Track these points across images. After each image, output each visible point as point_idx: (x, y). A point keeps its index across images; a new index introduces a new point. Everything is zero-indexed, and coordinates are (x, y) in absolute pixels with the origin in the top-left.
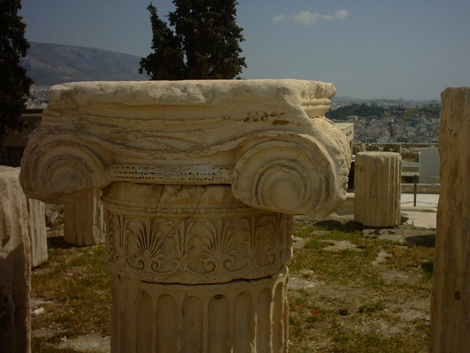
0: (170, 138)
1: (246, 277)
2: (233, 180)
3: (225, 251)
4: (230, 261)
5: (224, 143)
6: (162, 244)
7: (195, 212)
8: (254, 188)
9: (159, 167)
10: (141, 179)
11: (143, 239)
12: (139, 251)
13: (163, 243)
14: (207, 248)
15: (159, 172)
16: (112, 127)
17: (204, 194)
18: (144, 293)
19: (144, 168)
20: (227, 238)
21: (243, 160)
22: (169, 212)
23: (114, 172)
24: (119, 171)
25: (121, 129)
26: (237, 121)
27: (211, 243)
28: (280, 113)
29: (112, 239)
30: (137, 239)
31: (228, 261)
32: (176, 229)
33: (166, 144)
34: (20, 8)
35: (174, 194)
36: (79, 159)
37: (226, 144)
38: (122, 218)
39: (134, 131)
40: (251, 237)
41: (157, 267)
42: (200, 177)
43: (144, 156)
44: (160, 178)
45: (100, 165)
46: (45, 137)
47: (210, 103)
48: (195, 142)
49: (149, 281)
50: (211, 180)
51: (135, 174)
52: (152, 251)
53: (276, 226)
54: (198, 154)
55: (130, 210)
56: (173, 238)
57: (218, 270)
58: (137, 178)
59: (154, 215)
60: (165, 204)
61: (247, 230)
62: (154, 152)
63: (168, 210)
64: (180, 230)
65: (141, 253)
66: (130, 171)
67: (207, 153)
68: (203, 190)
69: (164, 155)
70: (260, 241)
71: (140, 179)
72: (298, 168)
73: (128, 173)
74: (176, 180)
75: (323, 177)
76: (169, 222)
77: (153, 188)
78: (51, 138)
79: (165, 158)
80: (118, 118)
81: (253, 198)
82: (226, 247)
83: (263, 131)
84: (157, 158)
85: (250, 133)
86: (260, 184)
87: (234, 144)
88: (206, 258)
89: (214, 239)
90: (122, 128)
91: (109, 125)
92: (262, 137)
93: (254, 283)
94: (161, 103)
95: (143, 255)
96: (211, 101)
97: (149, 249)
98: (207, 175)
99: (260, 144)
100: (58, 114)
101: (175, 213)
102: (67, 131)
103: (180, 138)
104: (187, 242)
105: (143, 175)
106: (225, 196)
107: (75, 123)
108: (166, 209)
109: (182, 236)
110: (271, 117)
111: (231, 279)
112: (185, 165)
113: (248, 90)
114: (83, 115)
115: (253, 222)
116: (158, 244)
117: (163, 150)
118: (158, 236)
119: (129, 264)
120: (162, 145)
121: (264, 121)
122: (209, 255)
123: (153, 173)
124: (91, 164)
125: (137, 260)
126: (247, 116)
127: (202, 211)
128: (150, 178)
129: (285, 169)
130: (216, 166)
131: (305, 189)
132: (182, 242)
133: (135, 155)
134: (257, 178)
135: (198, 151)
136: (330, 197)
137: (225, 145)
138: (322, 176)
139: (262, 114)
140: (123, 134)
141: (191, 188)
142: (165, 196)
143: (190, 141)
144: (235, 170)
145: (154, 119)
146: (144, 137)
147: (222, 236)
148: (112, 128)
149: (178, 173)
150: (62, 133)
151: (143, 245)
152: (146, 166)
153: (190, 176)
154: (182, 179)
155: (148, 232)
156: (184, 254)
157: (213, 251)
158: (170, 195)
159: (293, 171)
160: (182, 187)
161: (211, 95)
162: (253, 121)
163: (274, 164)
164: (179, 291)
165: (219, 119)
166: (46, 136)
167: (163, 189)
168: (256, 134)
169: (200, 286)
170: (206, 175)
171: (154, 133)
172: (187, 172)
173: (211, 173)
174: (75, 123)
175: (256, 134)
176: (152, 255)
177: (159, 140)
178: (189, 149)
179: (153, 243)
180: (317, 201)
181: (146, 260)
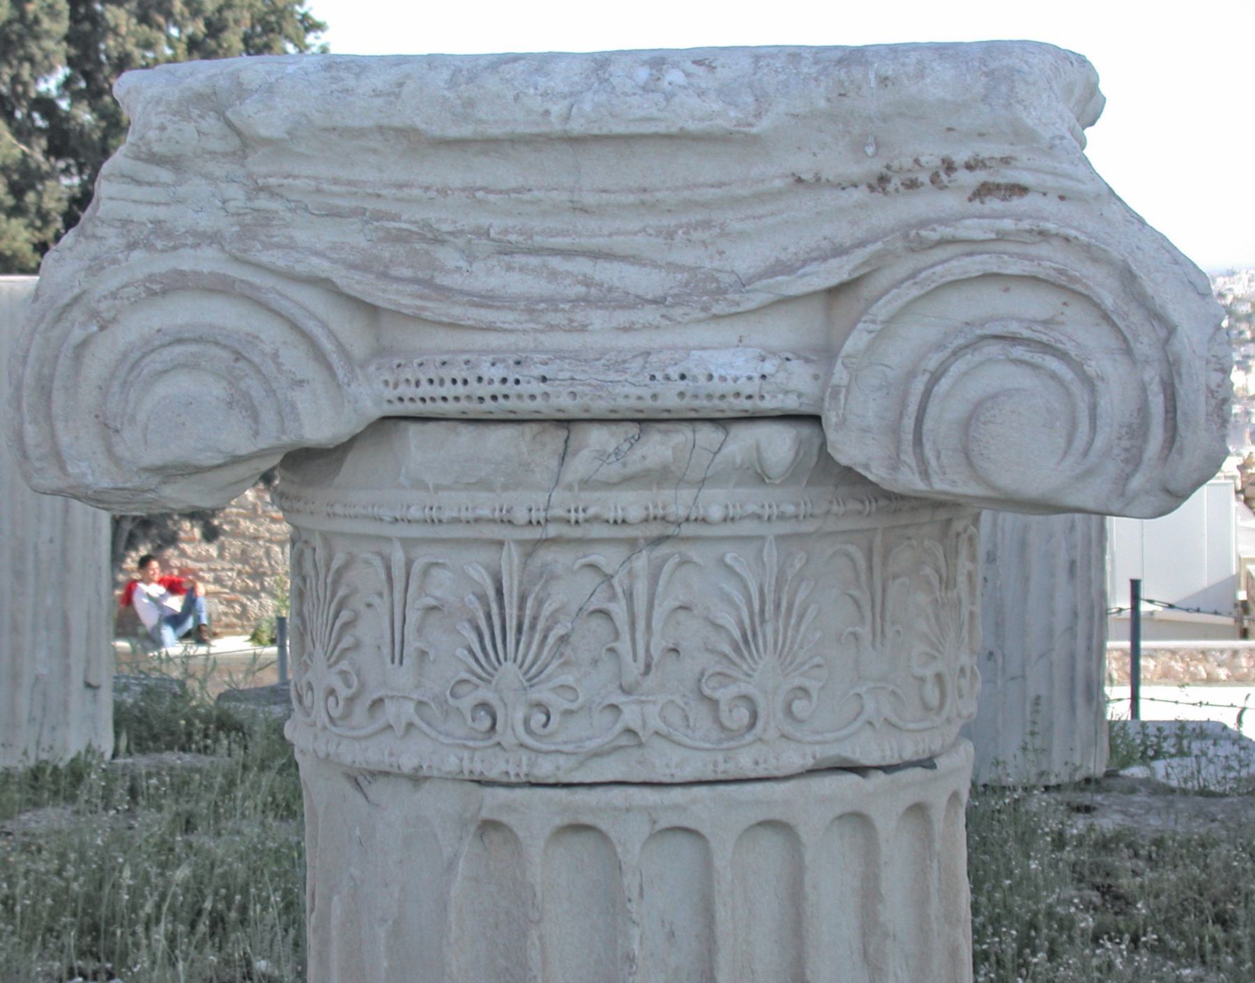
3: (789, 659)
6: (563, 639)
8: (909, 423)
9: (565, 358)
10: (501, 400)
15: (567, 375)
16: (377, 220)
19: (511, 362)
21: (872, 327)
23: (386, 383)
24: (409, 377)
25: (414, 228)
26: (843, 189)
27: (744, 636)
30: (467, 625)
33: (580, 277)
35: (616, 454)
36: (852, 560)
37: (808, 269)
39: (462, 232)
41: (545, 725)
43: (504, 323)
44: (573, 394)
46: (115, 261)
47: (750, 125)
48: (690, 268)
49: (513, 779)
52: (526, 665)
54: (705, 309)
55: (440, 521)
58: (481, 399)
59: (536, 533)
62: (543, 305)
65: (484, 675)
66: (455, 373)
69: (579, 316)
71: (493, 403)
73: (448, 383)
74: (632, 402)
75: (1152, 379)
77: (534, 437)
78: (143, 264)
79: (583, 328)
81: (903, 457)
83: (942, 221)
84: (552, 328)
85: (893, 231)
90: (416, 222)
91: (364, 214)
93: (879, 778)
95: (490, 682)
96: (751, 119)
97: (515, 661)
98: (743, 380)
100: (166, 175)
101: (615, 522)
103: (634, 257)
104: (657, 625)
105: (509, 388)
107: (232, 206)
108: (584, 510)
110: (967, 172)
113: (886, 78)
114: (265, 177)
116: (551, 640)
117: (573, 297)
118: (547, 609)
120: (568, 282)
121: (943, 188)
123: (544, 379)
125: (466, 703)
128: (533, 397)
133: (469, 319)
134: (919, 386)
135: (705, 298)
136: (1177, 444)
137: (804, 275)
143: (673, 267)
144: (839, 362)
145: (539, 189)
146: (500, 253)
148: (376, 224)
149: (641, 378)
150: (185, 245)
152: (515, 357)
153: (682, 385)
156: (648, 667)
157: (749, 660)
161: (750, 99)
162: (901, 189)
164: (628, 810)
166: (120, 256)
168: (917, 234)
169: (703, 791)
170: (739, 382)
172: (674, 372)
173: (756, 375)
174: (232, 206)
175: (917, 234)
176: (529, 680)
177: (555, 262)
178: (671, 292)
179: (531, 638)
180: (1134, 461)
181: (502, 699)
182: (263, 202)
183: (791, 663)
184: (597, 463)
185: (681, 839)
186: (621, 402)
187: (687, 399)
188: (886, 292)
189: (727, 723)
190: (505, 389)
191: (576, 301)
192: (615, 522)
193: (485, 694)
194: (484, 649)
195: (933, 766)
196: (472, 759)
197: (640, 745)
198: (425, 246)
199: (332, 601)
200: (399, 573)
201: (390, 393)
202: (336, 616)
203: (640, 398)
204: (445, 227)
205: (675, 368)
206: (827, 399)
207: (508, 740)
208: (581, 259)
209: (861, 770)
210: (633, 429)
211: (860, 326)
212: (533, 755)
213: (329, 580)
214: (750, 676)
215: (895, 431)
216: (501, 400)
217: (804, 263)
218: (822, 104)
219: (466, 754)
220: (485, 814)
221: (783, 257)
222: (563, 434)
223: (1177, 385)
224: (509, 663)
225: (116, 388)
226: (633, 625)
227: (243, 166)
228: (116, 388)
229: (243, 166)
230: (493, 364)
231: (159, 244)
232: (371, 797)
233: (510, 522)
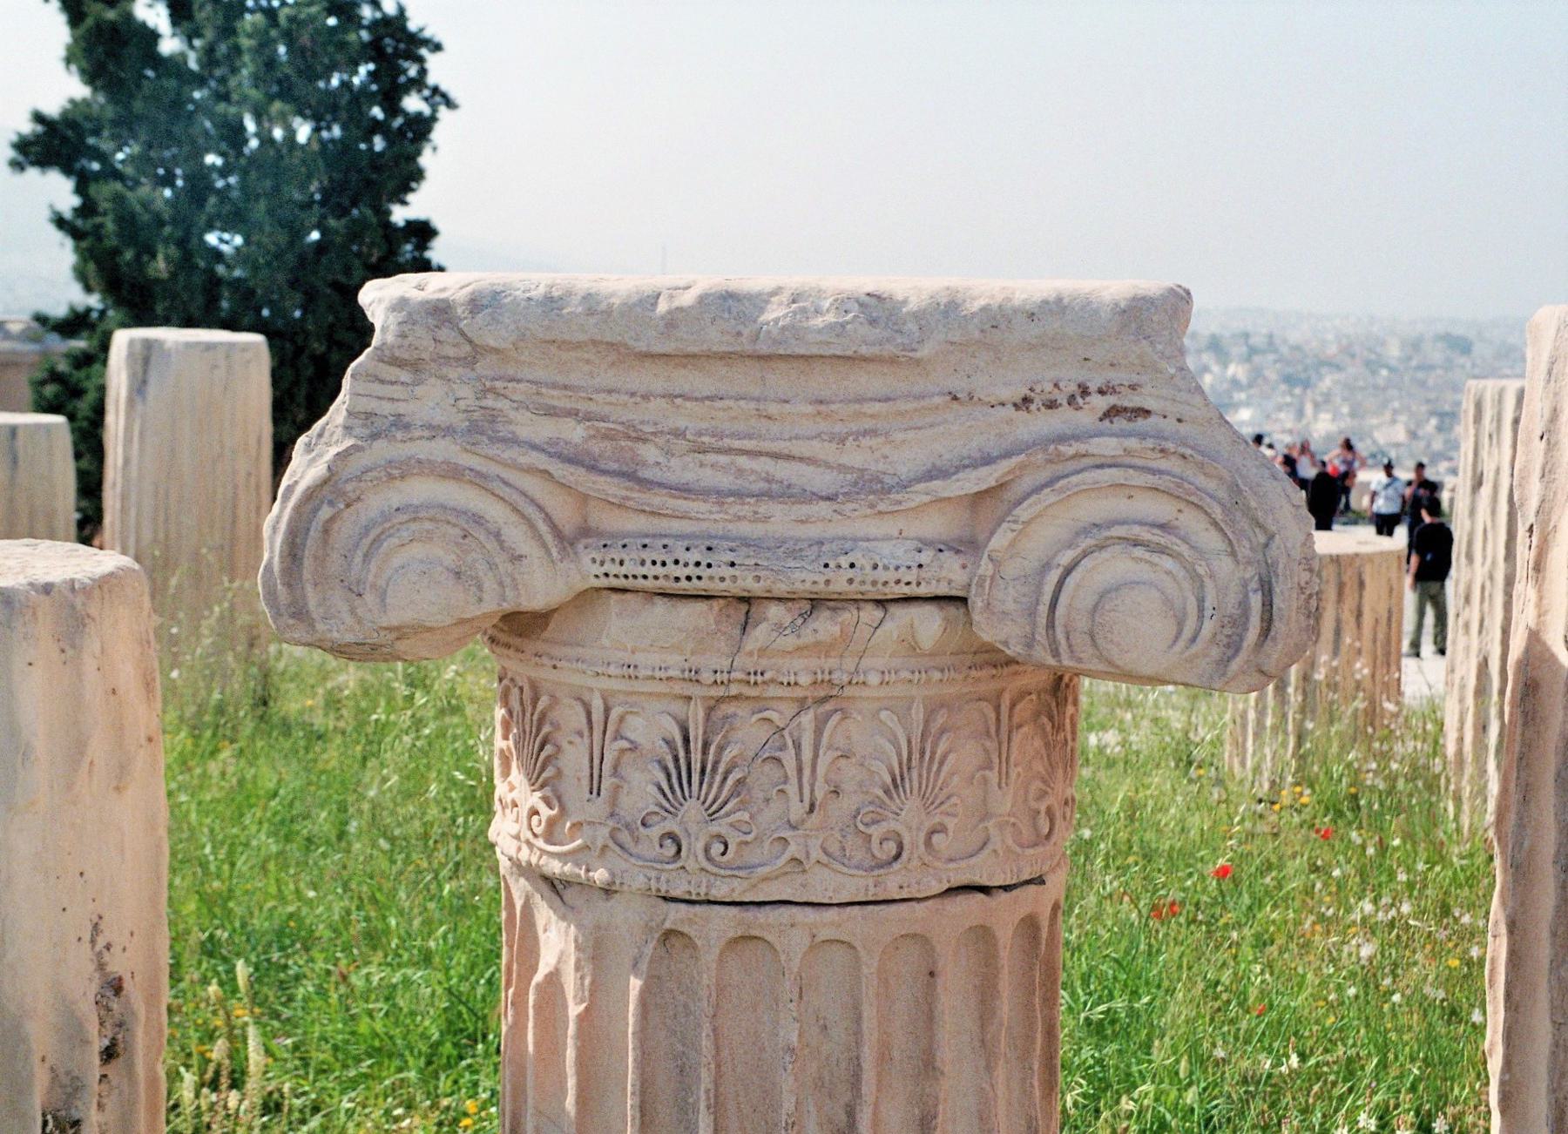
0: (776, 456)
2: (981, 585)
5: (954, 474)
8: (1043, 609)
10: (695, 580)
11: (678, 768)
12: (662, 807)
13: (745, 778)
14: (880, 793)
21: (1014, 526)
22: (772, 681)
23: (594, 561)
25: (620, 428)
27: (894, 780)
28: (1127, 384)
32: (786, 733)
33: (764, 475)
34: (1178, 302)
36: (478, 520)
41: (723, 854)
42: (881, 575)
44: (758, 578)
47: (913, 350)
49: (694, 897)
50: (914, 585)
51: (673, 567)
52: (702, 798)
54: (872, 506)
56: (778, 760)
59: (720, 692)
62: (732, 499)
64: (799, 738)
68: (879, 614)
69: (762, 509)
72: (1183, 549)
74: (808, 586)
75: (1253, 577)
79: (766, 519)
80: (610, 392)
81: (1038, 637)
82: (933, 789)
84: (740, 518)
86: (1063, 599)
87: (986, 477)
89: (900, 764)
91: (577, 415)
92: (1073, 457)
94: (757, 347)
96: (915, 345)
99: (1067, 476)
100: (405, 376)
101: (789, 684)
102: (436, 431)
104: (821, 770)
108: (762, 674)
109: (807, 754)
111: (946, 886)
112: (832, 540)
116: (730, 782)
118: (727, 756)
120: (752, 478)
123: (733, 564)
124: (516, 535)
125: (655, 832)
126: (1025, 391)
127: (874, 679)
128: (722, 579)
129: (1139, 552)
130: (923, 544)
132: (807, 772)
134: (1053, 577)
135: (871, 497)
136: (1272, 633)
138: (1250, 572)
139: (1073, 388)
140: (623, 444)
141: (844, 609)
142: (760, 635)
143: (842, 468)
144: (985, 556)
147: (922, 753)
149: (816, 565)
151: (676, 786)
152: (708, 543)
153: (851, 573)
155: (696, 743)
156: (811, 810)
157: (898, 801)
158: (779, 628)
159: (1164, 557)
160: (813, 607)
161: (915, 328)
162: (1043, 409)
163: (1107, 538)
164: (792, 926)
165: (937, 400)
167: (747, 612)
169: (857, 908)
171: (727, 442)
172: (844, 561)
174: (462, 404)
176: (710, 815)
177: (742, 461)
178: (842, 491)
179: (713, 778)
180: (1234, 646)
182: (490, 402)
183: (932, 803)
184: (775, 634)
185: (834, 947)
186: (799, 586)
187: (853, 586)
188: (1028, 495)
189: (876, 852)
190: (698, 571)
191: (759, 496)
192: (789, 684)
193: (671, 825)
194: (671, 787)
195: (1043, 882)
196: (658, 879)
197: (804, 871)
198: (629, 443)
199: (537, 736)
200: (597, 716)
201: (600, 571)
202: (541, 748)
204: (648, 429)
205: (846, 557)
206: (973, 586)
207: (691, 865)
209: (984, 890)
211: (1005, 525)
212: (712, 878)
213: (535, 717)
214: (897, 814)
215: (1032, 613)
216: (695, 580)
217: (958, 469)
218: (977, 334)
219: (653, 874)
220: (668, 925)
221: (938, 463)
223: (1274, 584)
224: (694, 799)
226: (800, 770)
227: (473, 370)
229: (473, 370)
230: (688, 549)
231: (399, 435)
232: (565, 898)
233: (697, 681)
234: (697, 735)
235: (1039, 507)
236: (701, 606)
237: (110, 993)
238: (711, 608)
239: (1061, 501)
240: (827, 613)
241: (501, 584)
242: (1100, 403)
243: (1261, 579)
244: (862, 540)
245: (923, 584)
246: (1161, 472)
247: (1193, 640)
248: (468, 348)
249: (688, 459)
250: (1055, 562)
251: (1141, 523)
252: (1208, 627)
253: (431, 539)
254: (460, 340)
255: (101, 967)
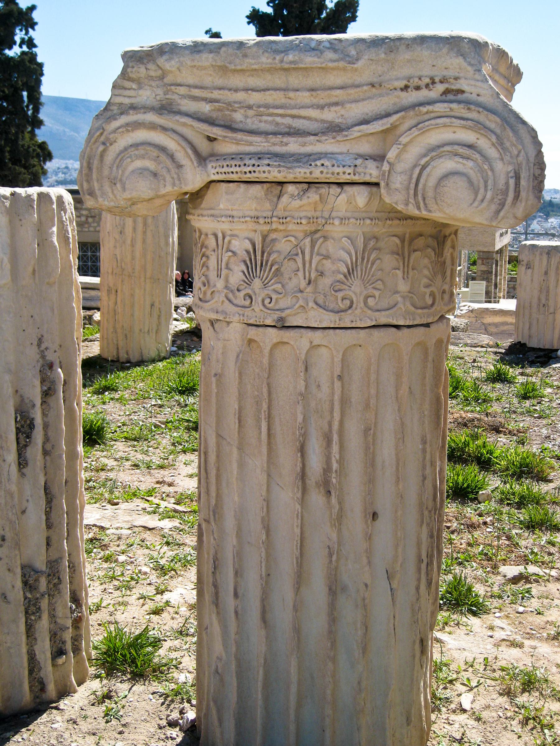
0: (293, 117)
1: (395, 322)
2: (383, 175)
4: (374, 297)
7: (326, 223)
8: (412, 186)
11: (251, 264)
14: (342, 276)
17: (340, 196)
18: (250, 341)
20: (370, 263)
21: (399, 146)
27: (349, 271)
29: (205, 268)
31: (371, 296)
32: (298, 247)
36: (163, 149)
38: (220, 236)
39: (243, 107)
40: (404, 264)
41: (270, 303)
45: (192, 156)
49: (258, 323)
53: (437, 251)
57: (356, 308)
58: (245, 173)
60: (284, 210)
61: (398, 254)
63: (288, 219)
67: (347, 136)
68: (339, 190)
69: (285, 140)
70: (415, 271)
74: (302, 175)
76: (290, 238)
79: (287, 144)
80: (220, 89)
81: (410, 200)
86: (422, 181)
88: (340, 290)
92: (427, 113)
93: (406, 330)
96: (354, 61)
101: (121, 733)
104: (313, 266)
106: (369, 201)
109: (307, 258)
115: (406, 243)
116: (273, 269)
119: (230, 301)
120: (282, 127)
121: (430, 90)
122: (344, 287)
123: (269, 165)
124: (180, 156)
125: (242, 294)
126: (404, 82)
128: (264, 172)
129: (457, 159)
131: (486, 186)
132: (307, 265)
134: (417, 171)
138: (510, 168)
139: (427, 80)
141: (322, 187)
142: (285, 199)
143: (323, 121)
147: (363, 259)
153: (322, 169)
154: (311, 173)
156: (309, 283)
174: (158, 98)
177: (278, 119)
179: (266, 268)
181: (254, 292)
184: (291, 199)
203: (305, 173)
208: (288, 118)
209: (397, 327)
210: (305, 186)
211: (395, 146)
215: (408, 189)
220: (249, 337)
222: (279, 188)
225: (115, 169)
228: (115, 169)
234: (259, 247)
235: (411, 137)
236: (258, 187)
237: (47, 368)
238: (263, 188)
239: (422, 133)
240: (314, 189)
241: (173, 178)
242: (441, 88)
243: (515, 172)
244: (330, 154)
245: (357, 175)
246: (467, 119)
247: (482, 201)
248: (160, 72)
249: (254, 119)
250: (419, 163)
251: (459, 144)
252: (489, 195)
253: (144, 158)
254: (157, 68)
255: (43, 357)
